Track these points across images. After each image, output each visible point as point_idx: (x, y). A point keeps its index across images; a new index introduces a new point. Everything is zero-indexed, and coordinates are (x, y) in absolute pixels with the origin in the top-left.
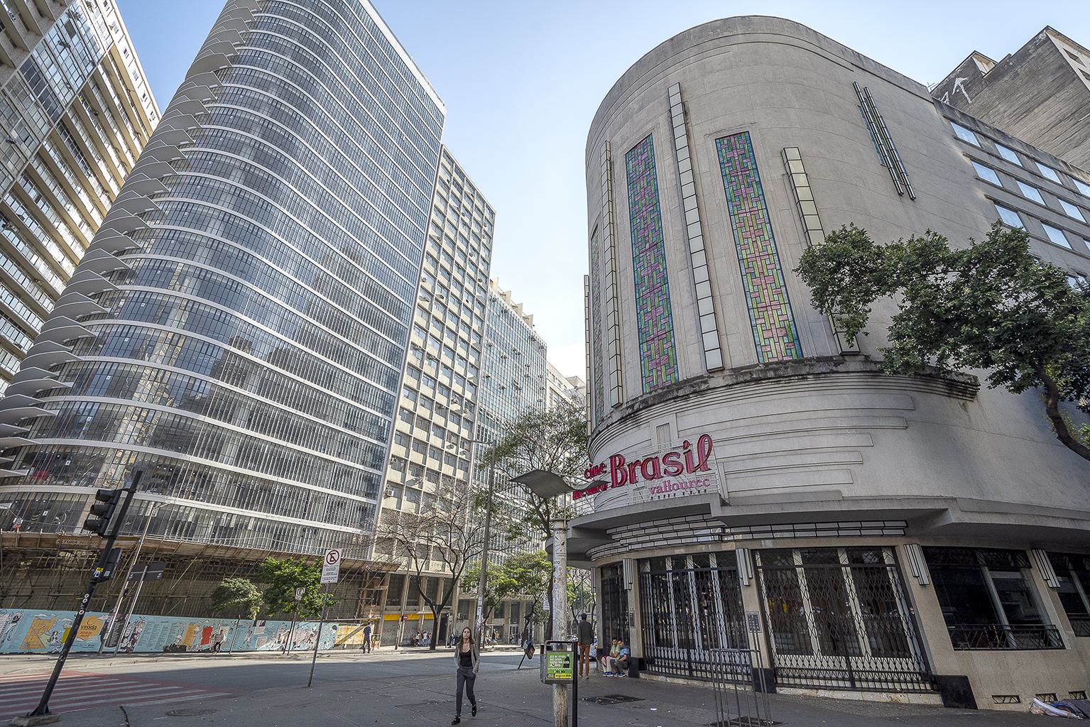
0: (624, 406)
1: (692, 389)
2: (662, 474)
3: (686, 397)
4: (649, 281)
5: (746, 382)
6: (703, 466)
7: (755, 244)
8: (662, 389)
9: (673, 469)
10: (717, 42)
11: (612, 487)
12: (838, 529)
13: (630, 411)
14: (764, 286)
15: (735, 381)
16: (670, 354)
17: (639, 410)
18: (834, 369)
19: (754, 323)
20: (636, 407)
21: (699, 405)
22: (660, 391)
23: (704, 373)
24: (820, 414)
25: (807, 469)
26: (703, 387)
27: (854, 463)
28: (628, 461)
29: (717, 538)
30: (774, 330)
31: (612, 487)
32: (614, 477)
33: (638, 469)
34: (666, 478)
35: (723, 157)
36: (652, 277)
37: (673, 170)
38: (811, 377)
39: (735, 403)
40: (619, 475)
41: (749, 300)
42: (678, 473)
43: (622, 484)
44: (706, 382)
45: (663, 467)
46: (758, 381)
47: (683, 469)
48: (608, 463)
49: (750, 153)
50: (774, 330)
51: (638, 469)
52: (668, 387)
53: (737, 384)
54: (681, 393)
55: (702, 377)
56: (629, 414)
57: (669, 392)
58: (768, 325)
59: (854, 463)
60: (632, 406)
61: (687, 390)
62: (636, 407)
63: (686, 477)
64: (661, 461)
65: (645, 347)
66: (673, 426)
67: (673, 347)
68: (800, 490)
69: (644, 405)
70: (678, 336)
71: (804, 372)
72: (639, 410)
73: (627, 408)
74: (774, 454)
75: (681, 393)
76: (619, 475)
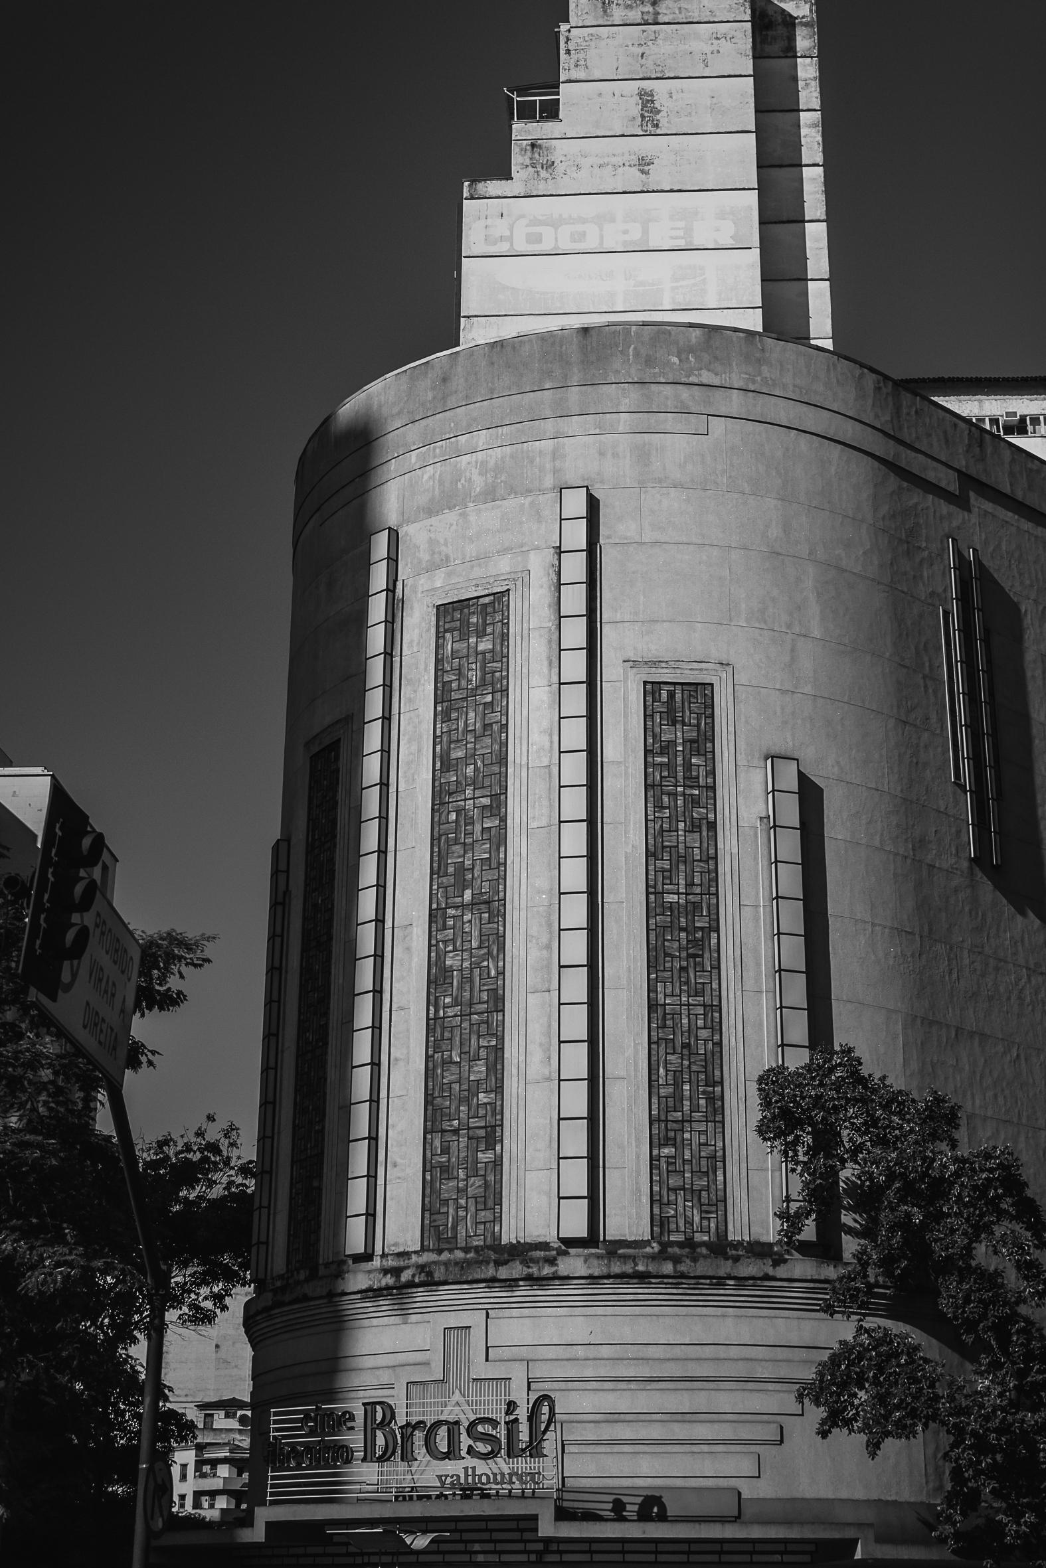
0: (377, 1262)
1: (526, 1271)
2: (464, 1453)
3: (511, 1284)
4: (461, 988)
5: (622, 1276)
6: (534, 1449)
7: (684, 974)
8: (466, 1250)
9: (482, 1448)
10: (685, 393)
11: (364, 1460)
12: (689, 1553)
13: (389, 1280)
14: (686, 1076)
15: (605, 1271)
16: (491, 1178)
17: (411, 1284)
18: (771, 1271)
19: (655, 1152)
20: (405, 1276)
21: (535, 1304)
22: (459, 1255)
23: (551, 1236)
24: (734, 1352)
25: (695, 1449)
26: (547, 1270)
27: (764, 1443)
28: (401, 1420)
29: (533, 1557)
30: (687, 1175)
31: (364, 1460)
32: (369, 1442)
33: (419, 1436)
34: (471, 1462)
35: (654, 737)
36: (471, 981)
37: (545, 724)
38: (732, 1282)
39: (600, 1311)
40: (380, 1440)
41: (655, 1100)
42: (492, 1454)
43: (383, 1459)
44: (552, 1262)
45: (465, 1441)
46: (642, 1278)
47: (500, 1449)
48: (359, 1413)
49: (703, 742)
50: (687, 1175)
51: (419, 1436)
52: (477, 1249)
53: (608, 1277)
54: (503, 1273)
55: (544, 1246)
56: (388, 1288)
57: (479, 1263)
58: (679, 1162)
59: (764, 1443)
60: (396, 1272)
61: (516, 1270)
62: (405, 1276)
63: (502, 1464)
64: (463, 1431)
65: (437, 1143)
66: (478, 1335)
67: (498, 1163)
68: (679, 1483)
69: (423, 1277)
70: (510, 1146)
71: (722, 1273)
72: (411, 1284)
73: (385, 1271)
74: (648, 1417)
75: (503, 1273)
76: (380, 1440)
